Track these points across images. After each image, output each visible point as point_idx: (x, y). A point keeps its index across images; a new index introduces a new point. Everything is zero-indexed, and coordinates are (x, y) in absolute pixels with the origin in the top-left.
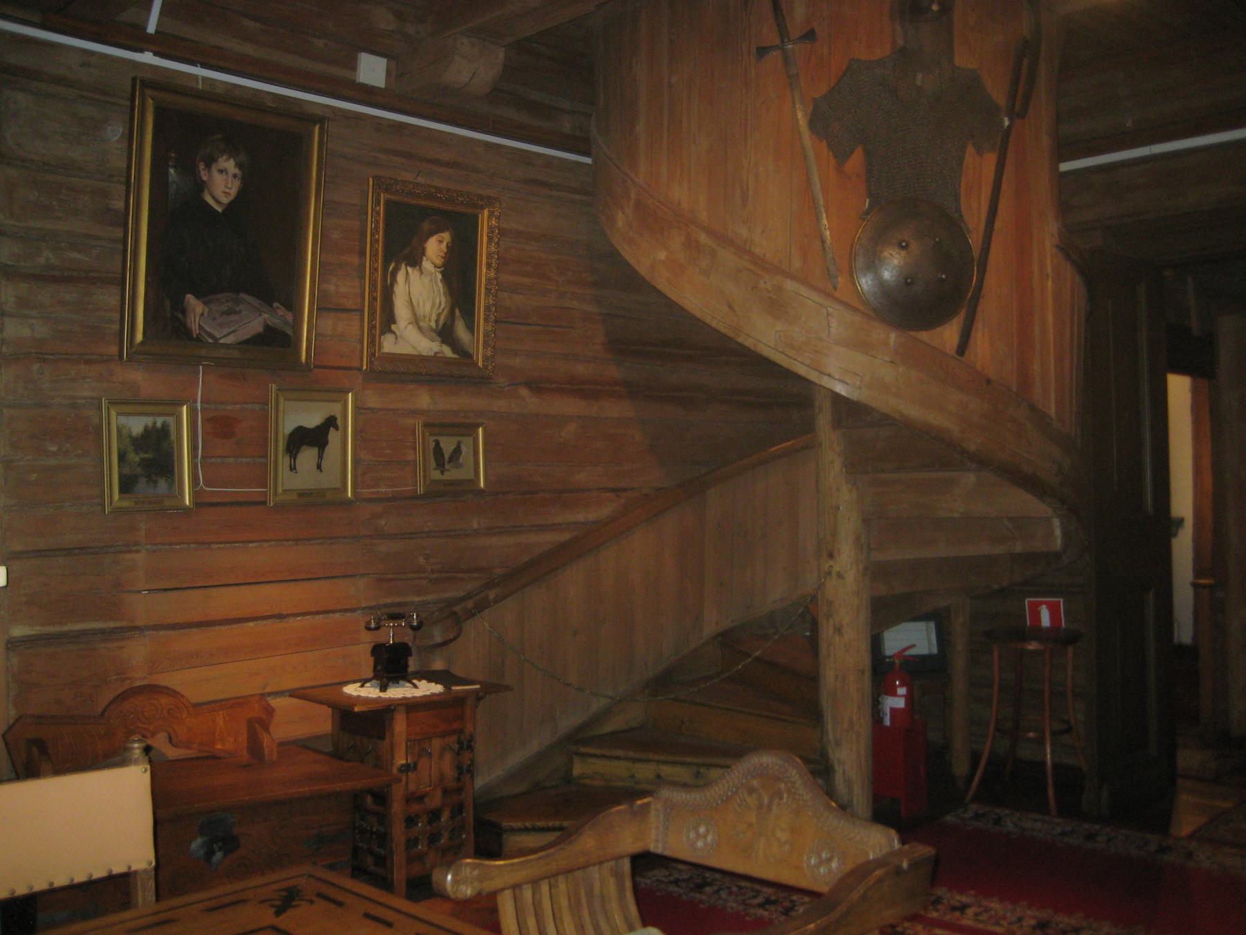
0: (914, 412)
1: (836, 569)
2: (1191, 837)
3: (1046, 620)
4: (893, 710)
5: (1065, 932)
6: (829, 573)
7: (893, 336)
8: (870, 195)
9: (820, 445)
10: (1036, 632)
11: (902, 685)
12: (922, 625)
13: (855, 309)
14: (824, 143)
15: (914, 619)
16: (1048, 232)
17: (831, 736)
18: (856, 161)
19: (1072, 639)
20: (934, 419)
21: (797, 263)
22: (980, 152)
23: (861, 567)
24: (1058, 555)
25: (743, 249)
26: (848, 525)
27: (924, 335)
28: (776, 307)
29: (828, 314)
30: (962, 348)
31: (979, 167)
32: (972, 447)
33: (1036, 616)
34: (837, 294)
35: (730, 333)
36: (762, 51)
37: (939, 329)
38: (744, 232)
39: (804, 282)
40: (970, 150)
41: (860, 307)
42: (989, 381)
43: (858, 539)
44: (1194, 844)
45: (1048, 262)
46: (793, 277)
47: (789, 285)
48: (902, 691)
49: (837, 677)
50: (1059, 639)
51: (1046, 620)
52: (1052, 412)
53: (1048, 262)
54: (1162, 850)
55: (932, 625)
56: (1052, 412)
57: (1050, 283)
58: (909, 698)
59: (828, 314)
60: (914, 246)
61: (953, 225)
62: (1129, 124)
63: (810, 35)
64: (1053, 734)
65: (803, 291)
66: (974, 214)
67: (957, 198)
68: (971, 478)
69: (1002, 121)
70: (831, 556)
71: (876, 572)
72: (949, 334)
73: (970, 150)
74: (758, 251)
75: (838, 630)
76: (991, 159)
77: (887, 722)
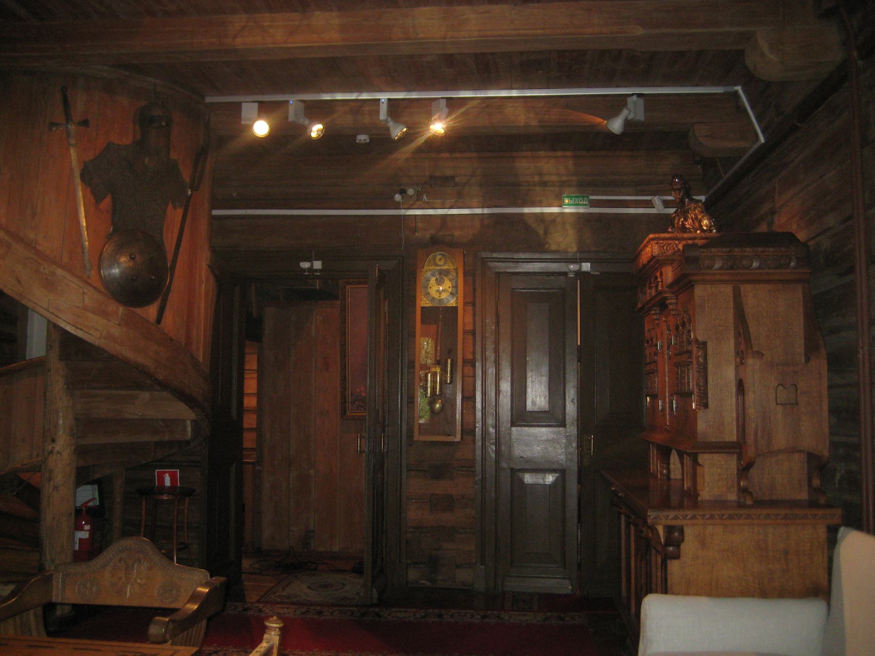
0: (128, 353)
1: (57, 448)
2: (258, 601)
3: (168, 482)
4: (80, 540)
5: (210, 654)
6: (52, 452)
7: (121, 309)
8: (113, 223)
9: (49, 370)
10: (162, 489)
11: (86, 524)
12: (89, 487)
13: (100, 292)
14: (89, 189)
15: (88, 483)
16: (204, 258)
17: (48, 557)
18: (107, 202)
19: (188, 493)
20: (141, 359)
21: (66, 260)
22: (174, 207)
23: (73, 448)
24: (188, 443)
25: (30, 246)
26: (63, 422)
27: (138, 311)
28: (50, 284)
29: (84, 293)
30: (159, 320)
31: (174, 215)
32: (161, 377)
33: (162, 480)
34: (90, 281)
35: (17, 297)
36: (52, 124)
37: (146, 308)
38: (32, 235)
39: (70, 271)
40: (170, 206)
41: (103, 290)
42: (171, 340)
43: (72, 430)
44: (261, 606)
45: (203, 273)
46: (62, 267)
47: (59, 271)
48: (87, 527)
49: (54, 519)
50: (183, 493)
51: (168, 482)
52: (201, 360)
53: (203, 273)
54: (245, 610)
55: (96, 487)
56: (201, 360)
57: (203, 286)
58: (92, 532)
59: (84, 293)
60: (138, 257)
61: (159, 247)
62: (235, 195)
63: (85, 123)
64: (178, 550)
65: (69, 276)
66: (169, 241)
67: (161, 233)
68: (146, 395)
69: (187, 192)
70: (53, 441)
71: (81, 451)
72: (151, 311)
73: (170, 206)
74: (40, 248)
75: (56, 488)
76: (180, 211)
77: (77, 548)
